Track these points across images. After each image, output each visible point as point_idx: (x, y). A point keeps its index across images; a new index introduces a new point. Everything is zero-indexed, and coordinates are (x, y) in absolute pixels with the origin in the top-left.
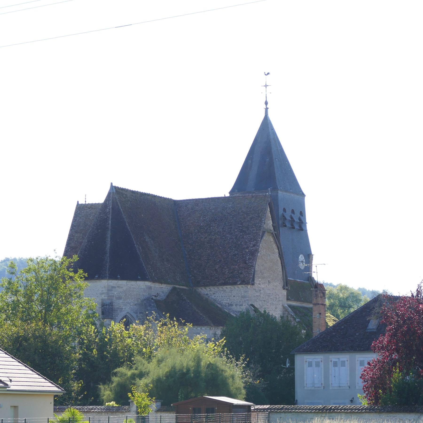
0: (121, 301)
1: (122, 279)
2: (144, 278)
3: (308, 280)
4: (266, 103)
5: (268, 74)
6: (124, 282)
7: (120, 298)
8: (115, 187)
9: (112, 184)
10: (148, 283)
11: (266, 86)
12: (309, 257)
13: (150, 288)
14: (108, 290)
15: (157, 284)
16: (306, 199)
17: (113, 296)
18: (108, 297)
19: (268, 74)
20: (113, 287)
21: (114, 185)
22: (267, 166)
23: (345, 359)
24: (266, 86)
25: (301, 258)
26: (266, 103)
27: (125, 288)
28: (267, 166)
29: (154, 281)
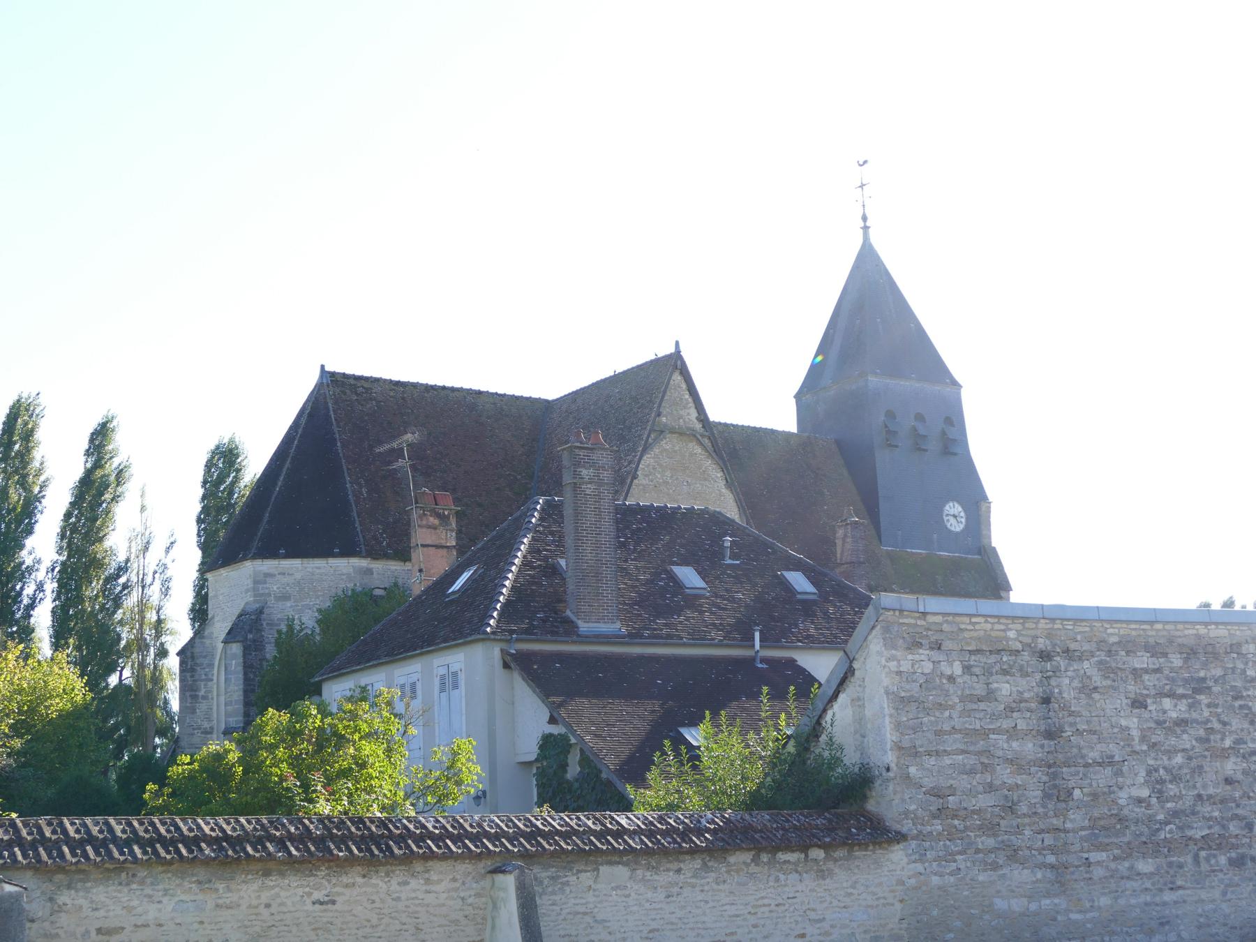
0: (289, 604)
1: (288, 556)
2: (348, 552)
3: (979, 553)
4: (864, 218)
5: (865, 162)
6: (296, 563)
7: (285, 597)
8: (333, 374)
9: (323, 367)
10: (363, 563)
11: (862, 186)
12: (976, 503)
13: (369, 571)
14: (256, 582)
15: (393, 563)
16: (963, 391)
17: (269, 595)
18: (255, 596)
19: (865, 162)
20: (267, 575)
21: (327, 369)
22: (872, 335)
23: (414, 678)
24: (862, 186)
25: (953, 508)
26: (864, 218)
27: (298, 576)
28: (872, 335)
29: (374, 554)
